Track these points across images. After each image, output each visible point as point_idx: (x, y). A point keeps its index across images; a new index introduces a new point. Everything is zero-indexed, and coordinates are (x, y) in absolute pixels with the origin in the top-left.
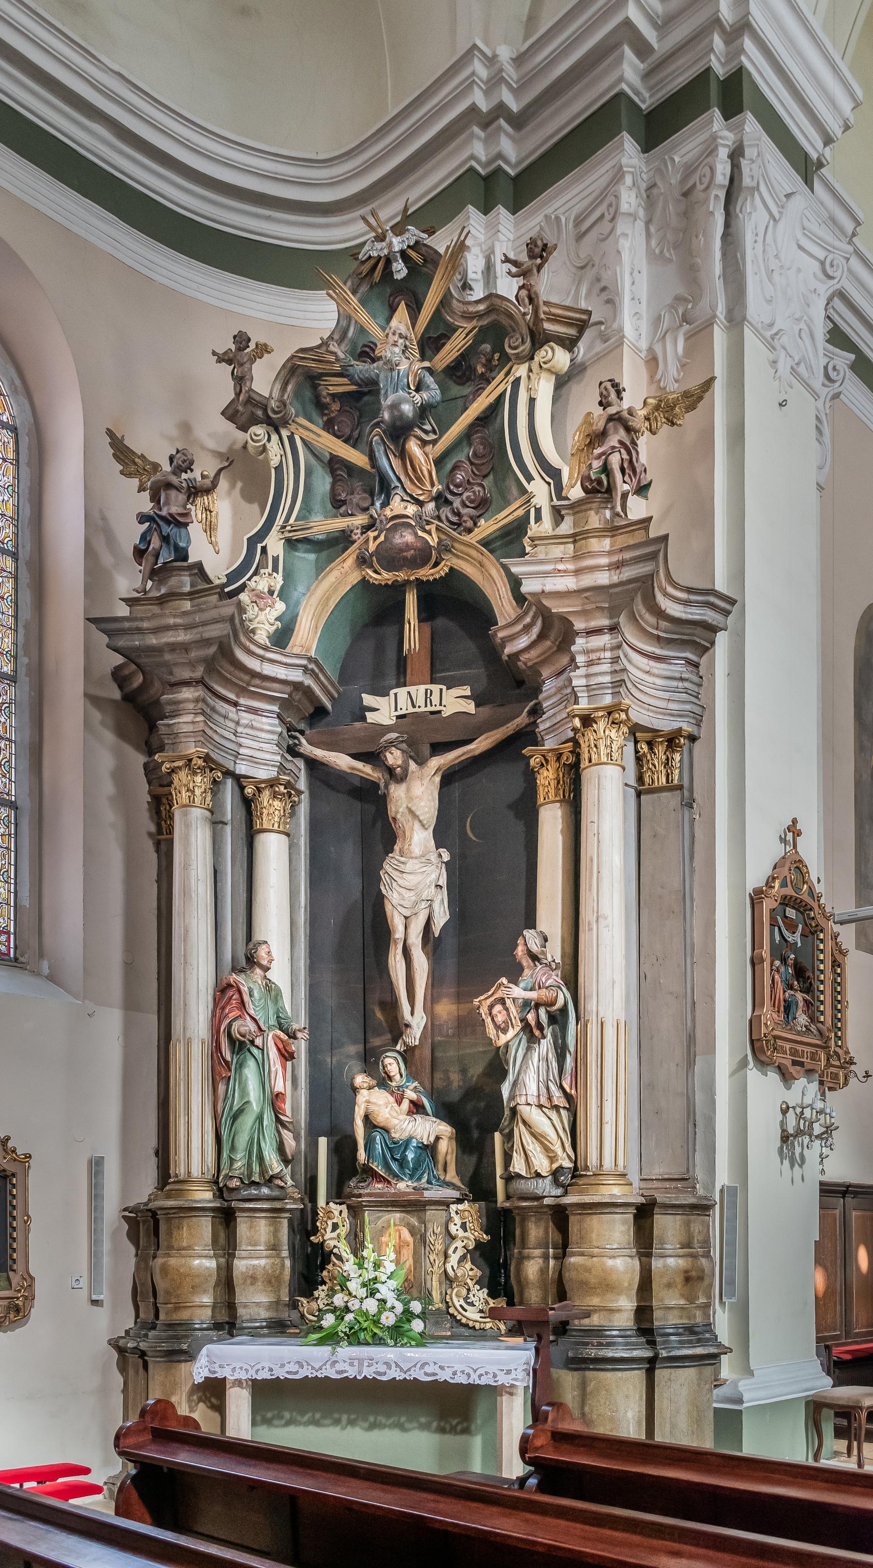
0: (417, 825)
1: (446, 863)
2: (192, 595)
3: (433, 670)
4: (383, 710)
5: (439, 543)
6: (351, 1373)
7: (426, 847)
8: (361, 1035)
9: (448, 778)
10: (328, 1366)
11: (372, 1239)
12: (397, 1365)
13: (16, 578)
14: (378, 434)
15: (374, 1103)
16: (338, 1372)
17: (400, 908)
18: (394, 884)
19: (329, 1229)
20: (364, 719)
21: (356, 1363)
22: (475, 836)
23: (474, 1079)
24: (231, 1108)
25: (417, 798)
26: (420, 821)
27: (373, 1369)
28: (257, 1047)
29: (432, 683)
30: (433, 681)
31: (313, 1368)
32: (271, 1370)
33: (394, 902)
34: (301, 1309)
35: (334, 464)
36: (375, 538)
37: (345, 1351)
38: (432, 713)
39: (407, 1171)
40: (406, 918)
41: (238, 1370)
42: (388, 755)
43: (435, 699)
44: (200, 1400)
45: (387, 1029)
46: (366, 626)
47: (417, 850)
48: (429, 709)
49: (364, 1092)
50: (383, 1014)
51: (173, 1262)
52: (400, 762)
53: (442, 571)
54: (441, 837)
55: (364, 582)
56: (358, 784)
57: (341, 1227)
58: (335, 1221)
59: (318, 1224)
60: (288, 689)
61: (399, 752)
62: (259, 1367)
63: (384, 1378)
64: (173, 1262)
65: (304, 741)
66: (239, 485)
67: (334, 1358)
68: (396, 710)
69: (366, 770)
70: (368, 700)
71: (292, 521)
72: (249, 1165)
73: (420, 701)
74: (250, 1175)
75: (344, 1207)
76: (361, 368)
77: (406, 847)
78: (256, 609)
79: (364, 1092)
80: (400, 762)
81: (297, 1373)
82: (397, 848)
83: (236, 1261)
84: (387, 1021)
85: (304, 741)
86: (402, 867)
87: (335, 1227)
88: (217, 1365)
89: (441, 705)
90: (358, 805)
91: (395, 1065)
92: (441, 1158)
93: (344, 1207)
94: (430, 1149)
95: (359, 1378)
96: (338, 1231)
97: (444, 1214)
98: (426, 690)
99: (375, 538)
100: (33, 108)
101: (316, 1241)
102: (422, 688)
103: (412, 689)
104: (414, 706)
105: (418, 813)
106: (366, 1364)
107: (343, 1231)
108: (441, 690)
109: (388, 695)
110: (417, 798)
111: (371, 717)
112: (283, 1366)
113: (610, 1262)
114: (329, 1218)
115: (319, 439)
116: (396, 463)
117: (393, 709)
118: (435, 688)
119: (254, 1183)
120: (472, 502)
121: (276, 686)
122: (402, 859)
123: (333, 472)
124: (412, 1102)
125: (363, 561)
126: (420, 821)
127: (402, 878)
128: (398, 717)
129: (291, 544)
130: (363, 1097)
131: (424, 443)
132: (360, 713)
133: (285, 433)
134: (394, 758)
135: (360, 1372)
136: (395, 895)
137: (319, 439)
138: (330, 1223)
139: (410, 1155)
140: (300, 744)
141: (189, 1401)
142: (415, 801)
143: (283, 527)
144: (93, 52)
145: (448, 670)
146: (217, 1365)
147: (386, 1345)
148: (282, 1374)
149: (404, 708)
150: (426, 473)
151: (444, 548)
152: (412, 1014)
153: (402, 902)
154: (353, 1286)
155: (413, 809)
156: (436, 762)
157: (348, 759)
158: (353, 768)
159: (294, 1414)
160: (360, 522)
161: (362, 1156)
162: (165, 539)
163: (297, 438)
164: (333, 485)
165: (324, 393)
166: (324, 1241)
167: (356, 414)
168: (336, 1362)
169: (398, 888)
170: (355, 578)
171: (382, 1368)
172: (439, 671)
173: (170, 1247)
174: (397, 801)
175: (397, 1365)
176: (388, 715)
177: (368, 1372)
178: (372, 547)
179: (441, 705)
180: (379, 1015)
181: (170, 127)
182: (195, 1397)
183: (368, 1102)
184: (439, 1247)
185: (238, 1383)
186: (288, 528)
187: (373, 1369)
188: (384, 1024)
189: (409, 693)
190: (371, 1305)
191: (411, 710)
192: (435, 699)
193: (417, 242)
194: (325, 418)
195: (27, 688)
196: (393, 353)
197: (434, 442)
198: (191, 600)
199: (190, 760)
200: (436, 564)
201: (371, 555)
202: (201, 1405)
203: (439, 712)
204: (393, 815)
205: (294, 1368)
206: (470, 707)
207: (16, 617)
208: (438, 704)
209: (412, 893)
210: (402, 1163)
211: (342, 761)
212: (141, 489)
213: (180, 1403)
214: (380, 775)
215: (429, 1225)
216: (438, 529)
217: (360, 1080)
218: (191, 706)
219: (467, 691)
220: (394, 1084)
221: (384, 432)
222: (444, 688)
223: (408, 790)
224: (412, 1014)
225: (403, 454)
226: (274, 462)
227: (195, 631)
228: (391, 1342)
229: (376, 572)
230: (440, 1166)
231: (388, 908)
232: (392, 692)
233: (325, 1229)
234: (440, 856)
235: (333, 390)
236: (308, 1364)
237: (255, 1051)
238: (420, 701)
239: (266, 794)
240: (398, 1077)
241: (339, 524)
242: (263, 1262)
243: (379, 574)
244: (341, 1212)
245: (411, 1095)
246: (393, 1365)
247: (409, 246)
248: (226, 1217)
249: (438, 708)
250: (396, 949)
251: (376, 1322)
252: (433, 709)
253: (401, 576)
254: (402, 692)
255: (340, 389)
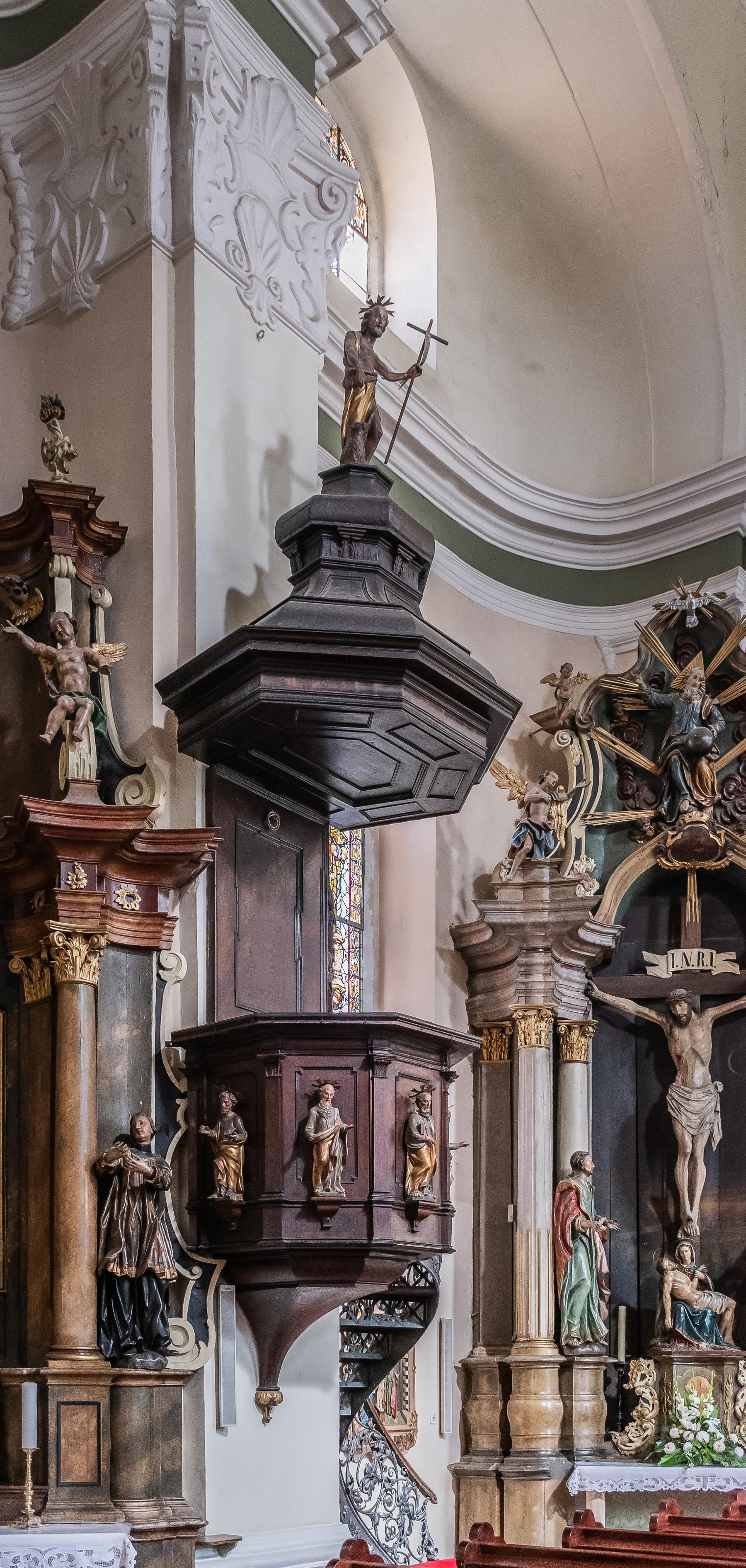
0: (698, 1062)
1: (720, 1094)
2: (551, 885)
3: (704, 935)
4: (663, 966)
5: (725, 845)
6: (697, 1487)
7: (705, 1080)
8: (635, 1223)
9: (718, 1022)
10: (679, 1481)
11: (679, 1387)
12: (735, 1481)
13: (363, 844)
14: (678, 754)
15: (680, 1282)
16: (687, 1486)
17: (688, 1129)
18: (682, 1109)
19: (639, 1378)
20: (645, 972)
21: (702, 1479)
22: (733, 1068)
23: (733, 1262)
24: (570, 1284)
25: (695, 1040)
26: (701, 1060)
27: (715, 1483)
28: (586, 1236)
29: (702, 947)
30: (703, 946)
31: (667, 1483)
32: (632, 1485)
33: (684, 1123)
34: (615, 1441)
35: (621, 764)
36: (673, 836)
37: (693, 1470)
38: (702, 971)
39: (705, 1334)
40: (693, 1136)
41: (605, 1485)
42: (677, 1006)
43: (707, 960)
44: (555, 1510)
45: (658, 1220)
46: (641, 895)
47: (698, 1082)
48: (701, 967)
49: (671, 1273)
50: (656, 1209)
51: (531, 1403)
52: (686, 1013)
53: (723, 863)
54: (717, 1070)
55: (656, 868)
56: (633, 1021)
57: (648, 1377)
58: (643, 1372)
59: (629, 1374)
60: (598, 950)
61: (686, 1005)
62: (622, 1482)
63: (725, 1490)
64: (531, 1403)
65: (595, 987)
66: (526, 767)
67: (684, 1476)
68: (673, 967)
69: (650, 1014)
70: (647, 956)
71: (592, 811)
72: (581, 1329)
73: (694, 961)
74: (585, 1337)
75: (651, 1362)
76: (656, 696)
77: (689, 1079)
78: (583, 889)
79: (671, 1273)
80: (686, 1013)
81: (653, 1487)
82: (679, 1078)
83: (574, 1403)
84: (658, 1213)
85: (595, 987)
86: (687, 1095)
87: (643, 1377)
88: (587, 1482)
89: (711, 965)
90: (632, 1039)
91: (689, 1252)
92: (724, 1325)
93: (651, 1362)
94: (718, 1319)
95: (704, 1490)
96: (646, 1380)
97: (734, 1368)
98: (699, 953)
99: (673, 836)
100: (400, 466)
101: (627, 1388)
102: (696, 951)
103: (687, 951)
104: (688, 965)
105: (701, 1053)
106: (709, 1480)
107: (650, 1380)
108: (712, 954)
109: (666, 954)
110: (695, 1040)
111: (650, 971)
112: (642, 1481)
113: (544, 1404)
114: (639, 1370)
115: (615, 746)
116: (688, 776)
117: (671, 966)
118: (707, 952)
119: (589, 1342)
120: (742, 808)
121: (590, 948)
122: (687, 1089)
123: (620, 771)
124: (700, 1281)
125: (658, 852)
126: (701, 1060)
127: (688, 1104)
128: (673, 972)
129: (590, 830)
130: (670, 1277)
131: (710, 760)
132: (641, 967)
133: (585, 738)
134: (681, 1009)
135: (705, 1486)
136: (683, 1117)
137: (615, 746)
138: (639, 1374)
139: (707, 1321)
140: (592, 989)
141: (548, 1510)
142: (699, 1043)
143: (584, 816)
144: (461, 433)
145: (712, 936)
146: (587, 1482)
147: (723, 1466)
148: (641, 1488)
149: (680, 966)
150: (710, 784)
151: (727, 847)
152: (691, 1209)
153: (689, 1124)
154: (685, 1422)
155: (697, 1050)
156: (712, 1012)
157: (634, 1004)
158: (639, 1012)
159: (623, 1521)
160: (648, 815)
161: (669, 1322)
162: (536, 842)
163: (596, 743)
164: (620, 781)
165: (620, 709)
166: (634, 1388)
167: (642, 726)
168: (686, 1478)
169: (685, 1112)
170: (650, 863)
171: (723, 1483)
172: (710, 939)
173: (528, 1392)
174: (682, 1043)
175: (735, 1481)
176: (665, 970)
177: (711, 1486)
178: (670, 842)
179: (711, 965)
180: (651, 1207)
181: (437, 432)
182: (552, 1508)
183: (674, 1281)
184: (731, 1393)
185: (598, 1495)
186: (589, 817)
187: (715, 1483)
188: (656, 1215)
189: (684, 954)
190: (703, 1436)
191: (686, 968)
192: (707, 960)
193: (711, 603)
194: (613, 725)
195: (372, 935)
196: (692, 692)
197: (716, 761)
198: (550, 888)
199: (539, 1011)
200: (720, 859)
201: (667, 848)
202: (556, 1513)
203: (710, 971)
204: (678, 1053)
205: (651, 1483)
206: (736, 969)
207: (363, 876)
208: (709, 964)
209: (697, 1117)
210: (701, 1328)
211: (629, 1006)
212: (511, 798)
213: (540, 1513)
214: (664, 1020)
215: (726, 1377)
216: (726, 834)
217: (667, 1263)
218: (541, 968)
219: (733, 956)
220: (685, 1266)
221: (682, 751)
222: (714, 952)
223: (691, 1034)
224: (691, 1209)
225: (694, 770)
226: (577, 759)
227: (558, 914)
228: (727, 1464)
229: (668, 860)
230: (722, 1331)
231: (678, 1129)
232: (670, 952)
233: (635, 1379)
234: (716, 1087)
235: (628, 708)
236: (663, 1480)
237: (584, 1239)
238: (694, 961)
239: (575, 1033)
240: (689, 1261)
241: (631, 815)
242: (587, 1404)
243: (672, 862)
244: (649, 1365)
245: (700, 1275)
246: (732, 1481)
247: (704, 606)
248: (565, 1369)
249: (709, 968)
250: (685, 1160)
251: (711, 1449)
252: (705, 968)
253: (688, 865)
254: (678, 953)
255: (634, 708)
